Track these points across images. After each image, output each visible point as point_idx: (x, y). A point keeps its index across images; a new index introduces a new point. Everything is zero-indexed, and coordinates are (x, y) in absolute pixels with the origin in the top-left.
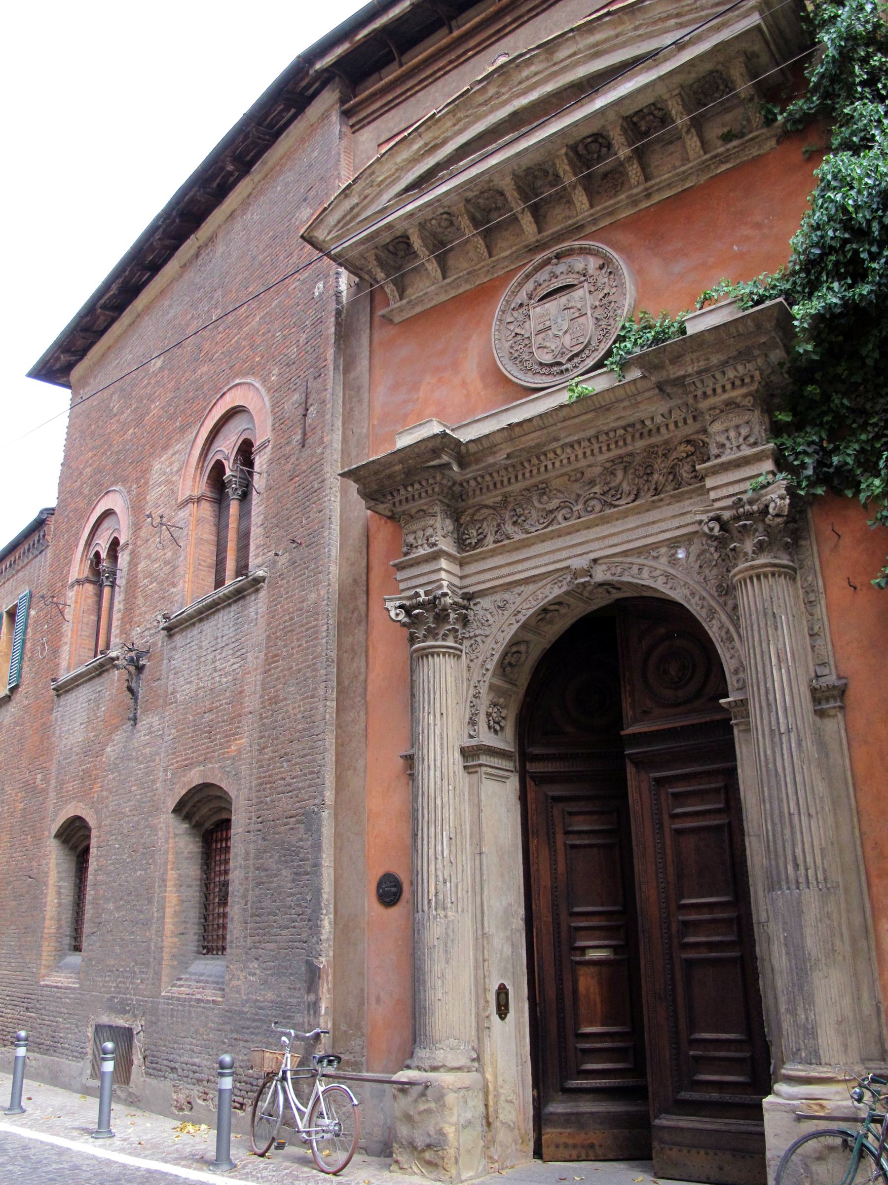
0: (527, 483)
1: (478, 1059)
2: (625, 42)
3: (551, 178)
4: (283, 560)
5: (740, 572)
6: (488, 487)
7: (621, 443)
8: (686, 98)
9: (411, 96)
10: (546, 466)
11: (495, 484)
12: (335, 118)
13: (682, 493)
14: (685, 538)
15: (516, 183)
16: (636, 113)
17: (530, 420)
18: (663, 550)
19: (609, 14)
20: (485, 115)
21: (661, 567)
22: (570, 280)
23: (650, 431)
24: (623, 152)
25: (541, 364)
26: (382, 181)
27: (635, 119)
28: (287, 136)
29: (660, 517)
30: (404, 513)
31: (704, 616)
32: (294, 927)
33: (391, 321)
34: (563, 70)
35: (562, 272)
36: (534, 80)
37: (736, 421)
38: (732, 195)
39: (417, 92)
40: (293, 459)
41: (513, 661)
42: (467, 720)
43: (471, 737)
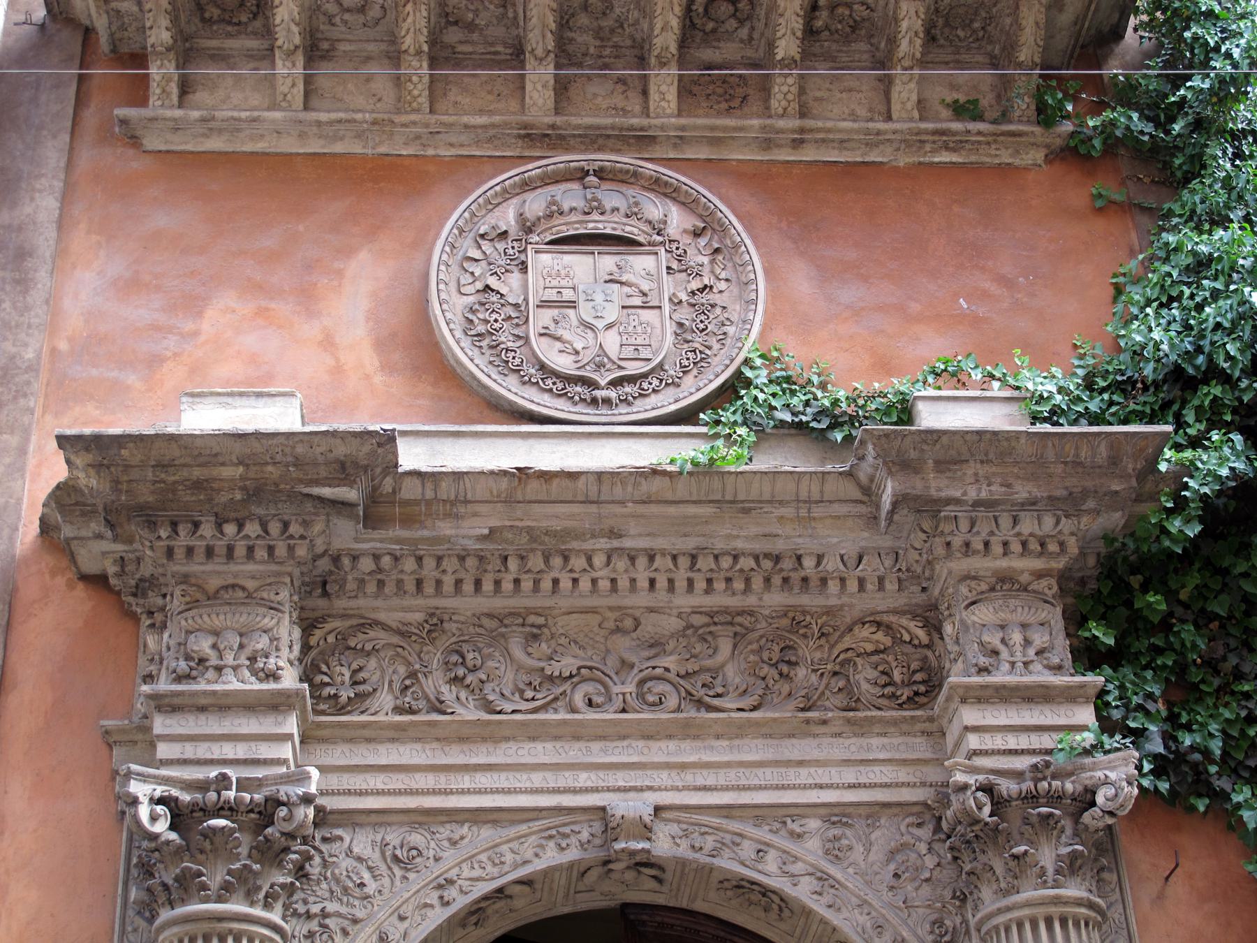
5: (1028, 904)
7: (739, 585)
10: (556, 582)
17: (573, 476)
21: (811, 859)
22: (632, 229)
23: (805, 580)
25: (543, 367)
29: (816, 754)
30: (185, 579)
33: (134, 141)
35: (615, 209)
37: (1022, 615)
38: (956, 209)
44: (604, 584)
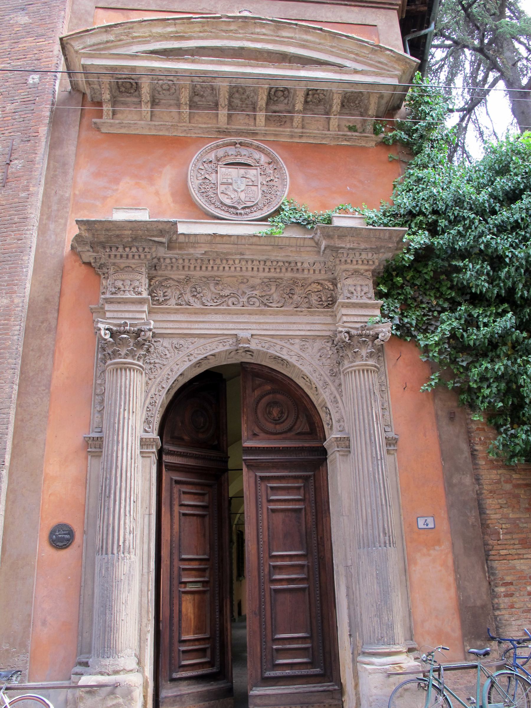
0: (207, 274)
2: (322, 50)
3: (244, 97)
10: (224, 268)
14: (311, 337)
17: (230, 236)
18: (297, 341)
19: (296, 25)
20: (223, 38)
22: (249, 162)
23: (298, 269)
25: (222, 203)
26: (136, 37)
27: (310, 92)
29: (299, 321)
30: (114, 264)
33: (98, 129)
34: (282, 43)
36: (262, 37)
42: (143, 420)
43: (146, 431)
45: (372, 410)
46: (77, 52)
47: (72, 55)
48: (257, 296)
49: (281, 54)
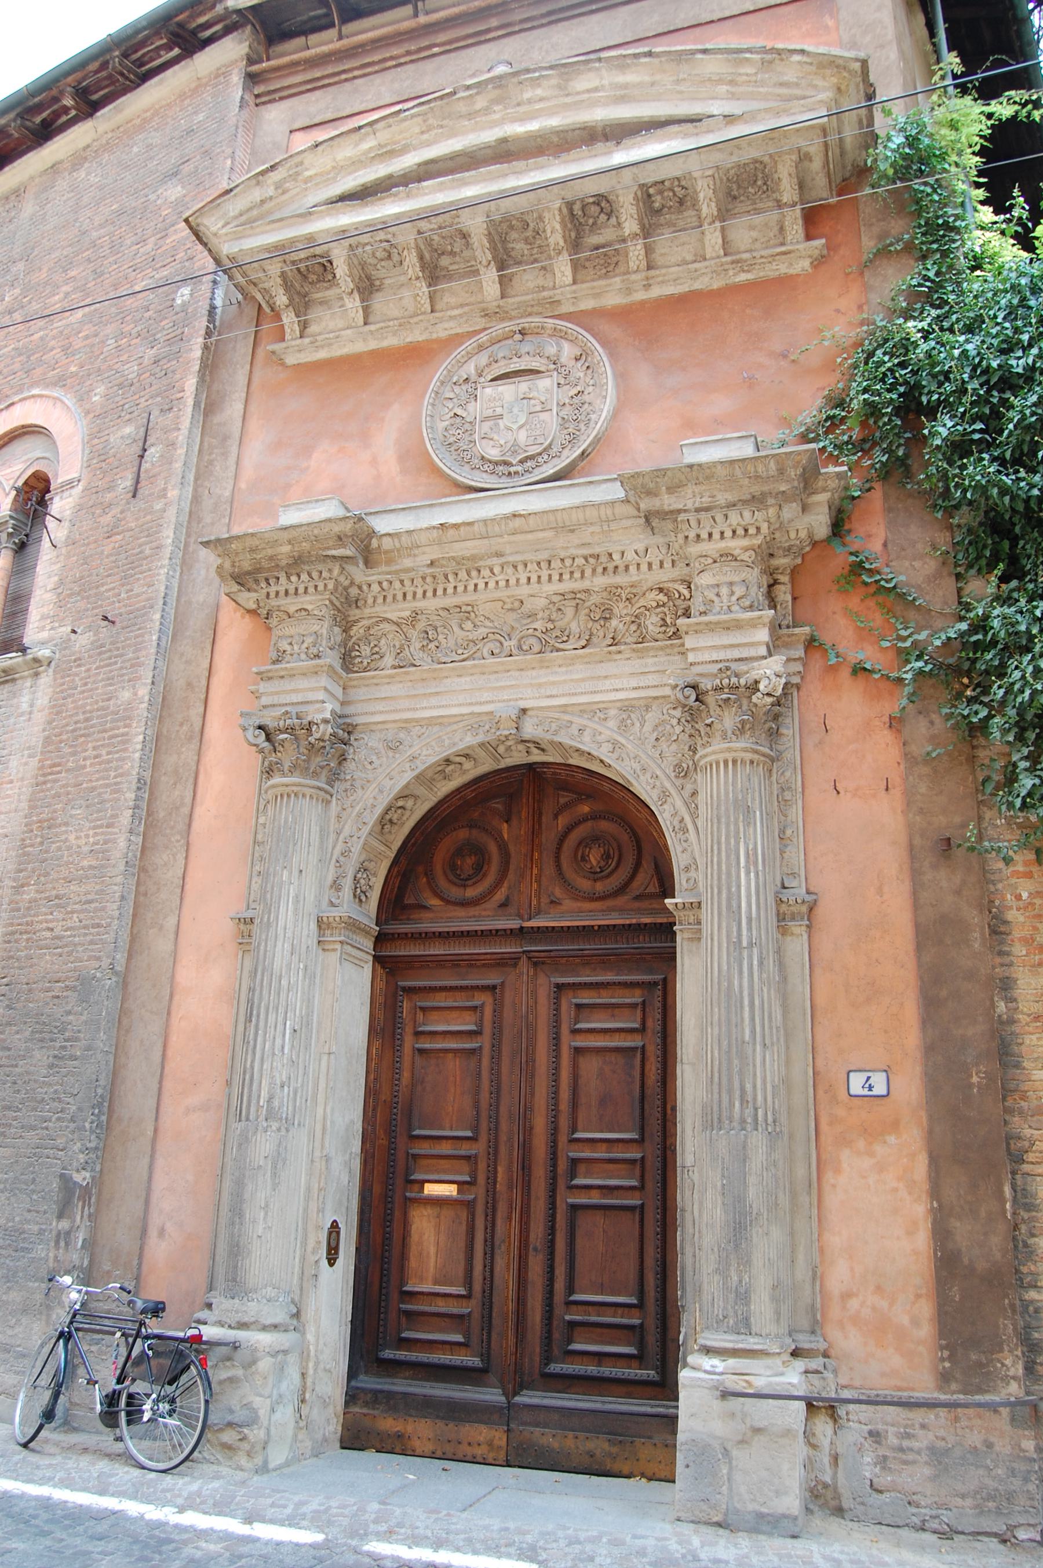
1: (297, 1315)
3: (529, 233)
4: (83, 640)
5: (714, 753)
6: (394, 596)
7: (577, 575)
8: (718, 182)
9: (346, 80)
10: (476, 585)
11: (405, 595)
12: (236, 79)
13: (647, 649)
15: (488, 228)
16: (656, 183)
17: (470, 524)
22: (534, 365)
23: (616, 567)
24: (630, 226)
27: (651, 191)
28: (161, 82)
31: (655, 798)
32: (47, 1128)
38: (748, 311)
39: (355, 78)
40: (115, 511)
41: (395, 818)
43: (332, 904)
44: (502, 584)
45: (737, 843)
46: (215, 235)
47: (213, 242)
48: (537, 633)
49: (584, 129)
